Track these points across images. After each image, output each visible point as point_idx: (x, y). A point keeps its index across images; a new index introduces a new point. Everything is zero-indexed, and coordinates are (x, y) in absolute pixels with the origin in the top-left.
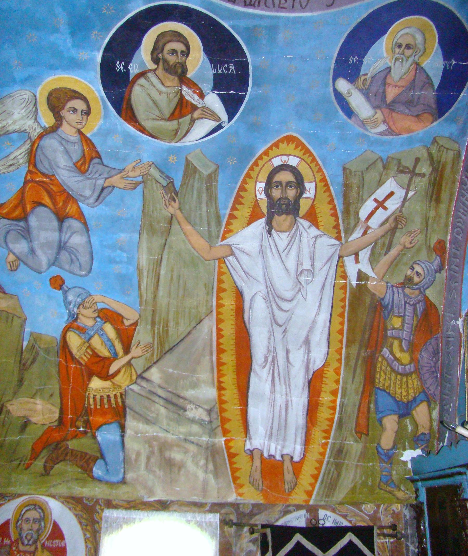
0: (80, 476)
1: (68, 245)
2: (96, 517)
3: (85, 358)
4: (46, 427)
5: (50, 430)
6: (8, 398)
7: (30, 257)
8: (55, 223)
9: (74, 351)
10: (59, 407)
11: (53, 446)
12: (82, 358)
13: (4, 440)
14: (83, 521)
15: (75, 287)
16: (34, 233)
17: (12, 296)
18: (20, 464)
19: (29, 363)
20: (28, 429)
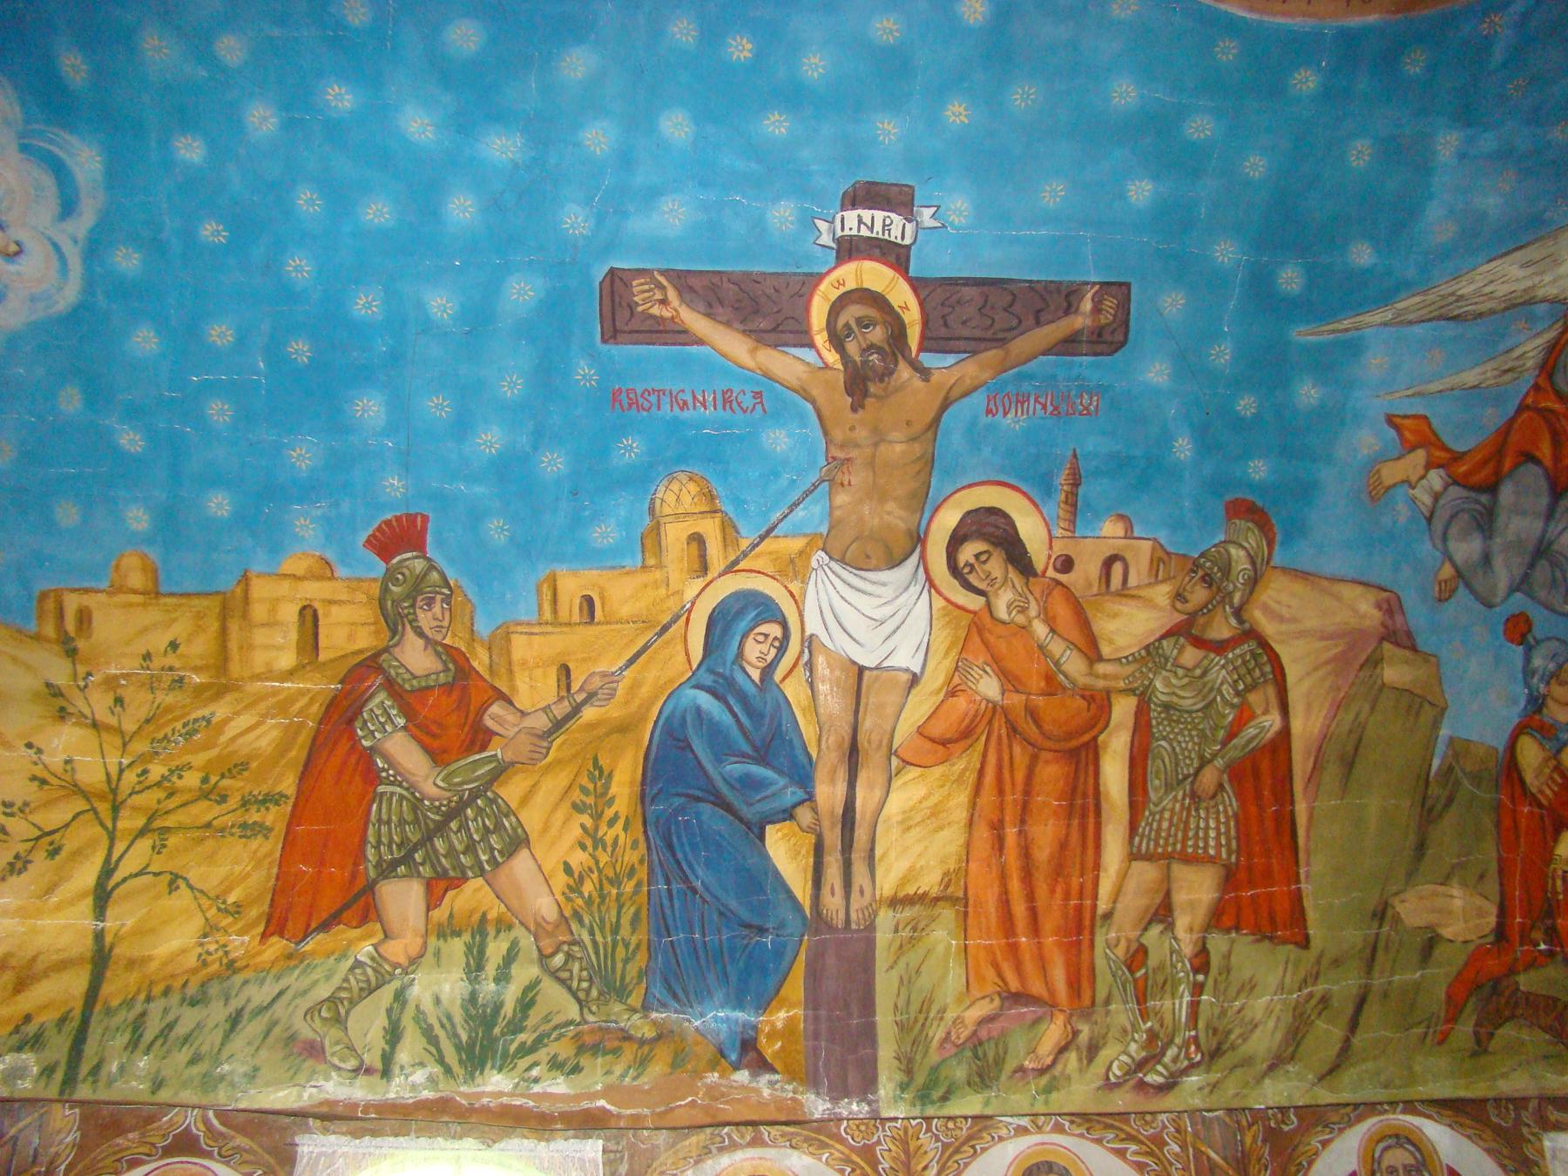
0: (1552, 1050)
1: (1555, 547)
2: (1529, 1151)
3: (1548, 792)
4: (1471, 947)
5: (1478, 956)
6: (1394, 889)
7: (1480, 571)
8: (1544, 501)
9: (1529, 777)
10: (1497, 899)
11: (1487, 990)
12: (1541, 792)
13: (1390, 983)
14: (1506, 1162)
15: (1549, 639)
16: (1501, 521)
17: (1427, 657)
18: (1426, 1034)
19: (1439, 807)
20: (1437, 952)
